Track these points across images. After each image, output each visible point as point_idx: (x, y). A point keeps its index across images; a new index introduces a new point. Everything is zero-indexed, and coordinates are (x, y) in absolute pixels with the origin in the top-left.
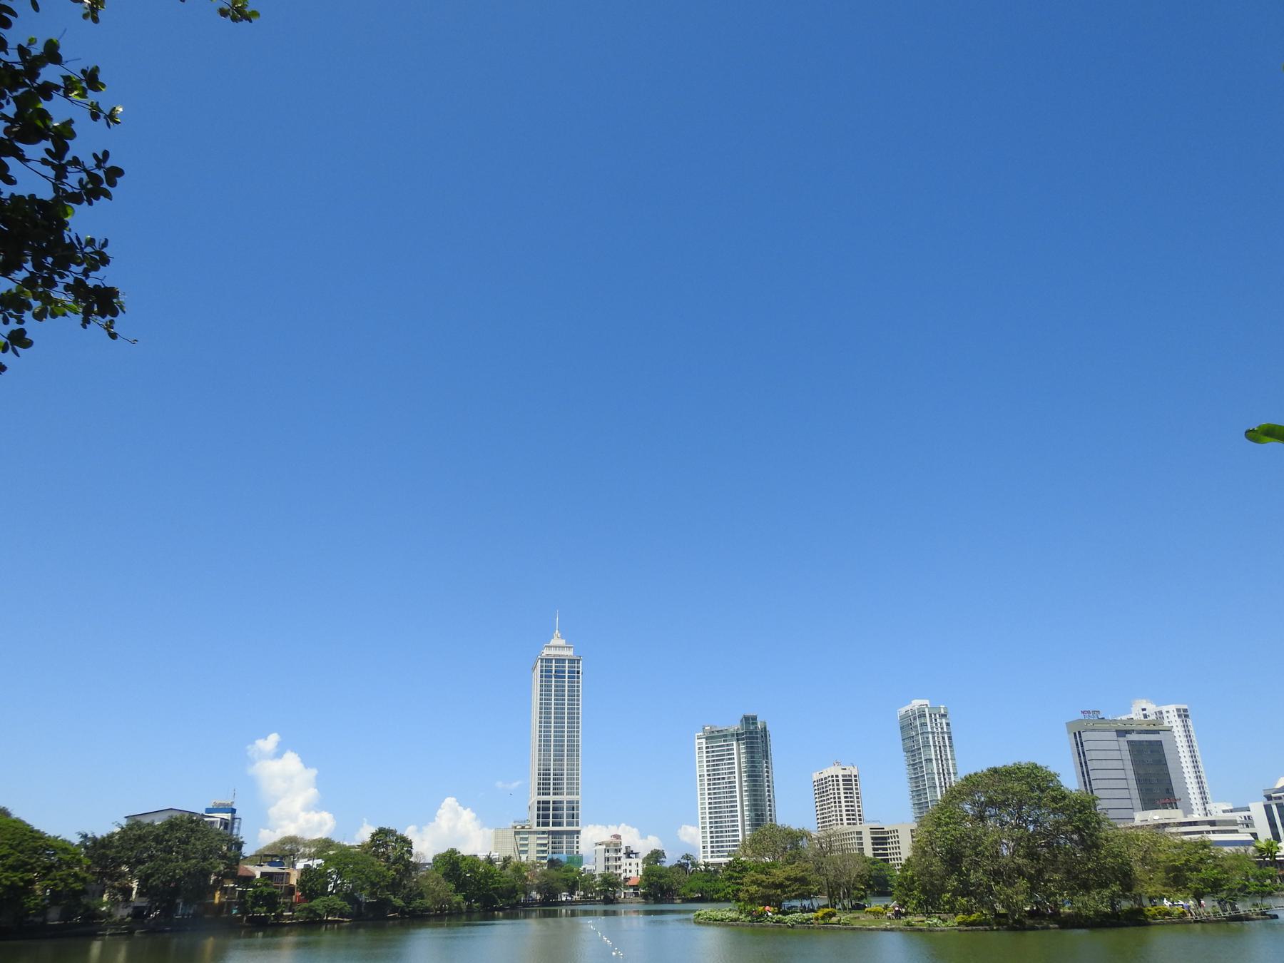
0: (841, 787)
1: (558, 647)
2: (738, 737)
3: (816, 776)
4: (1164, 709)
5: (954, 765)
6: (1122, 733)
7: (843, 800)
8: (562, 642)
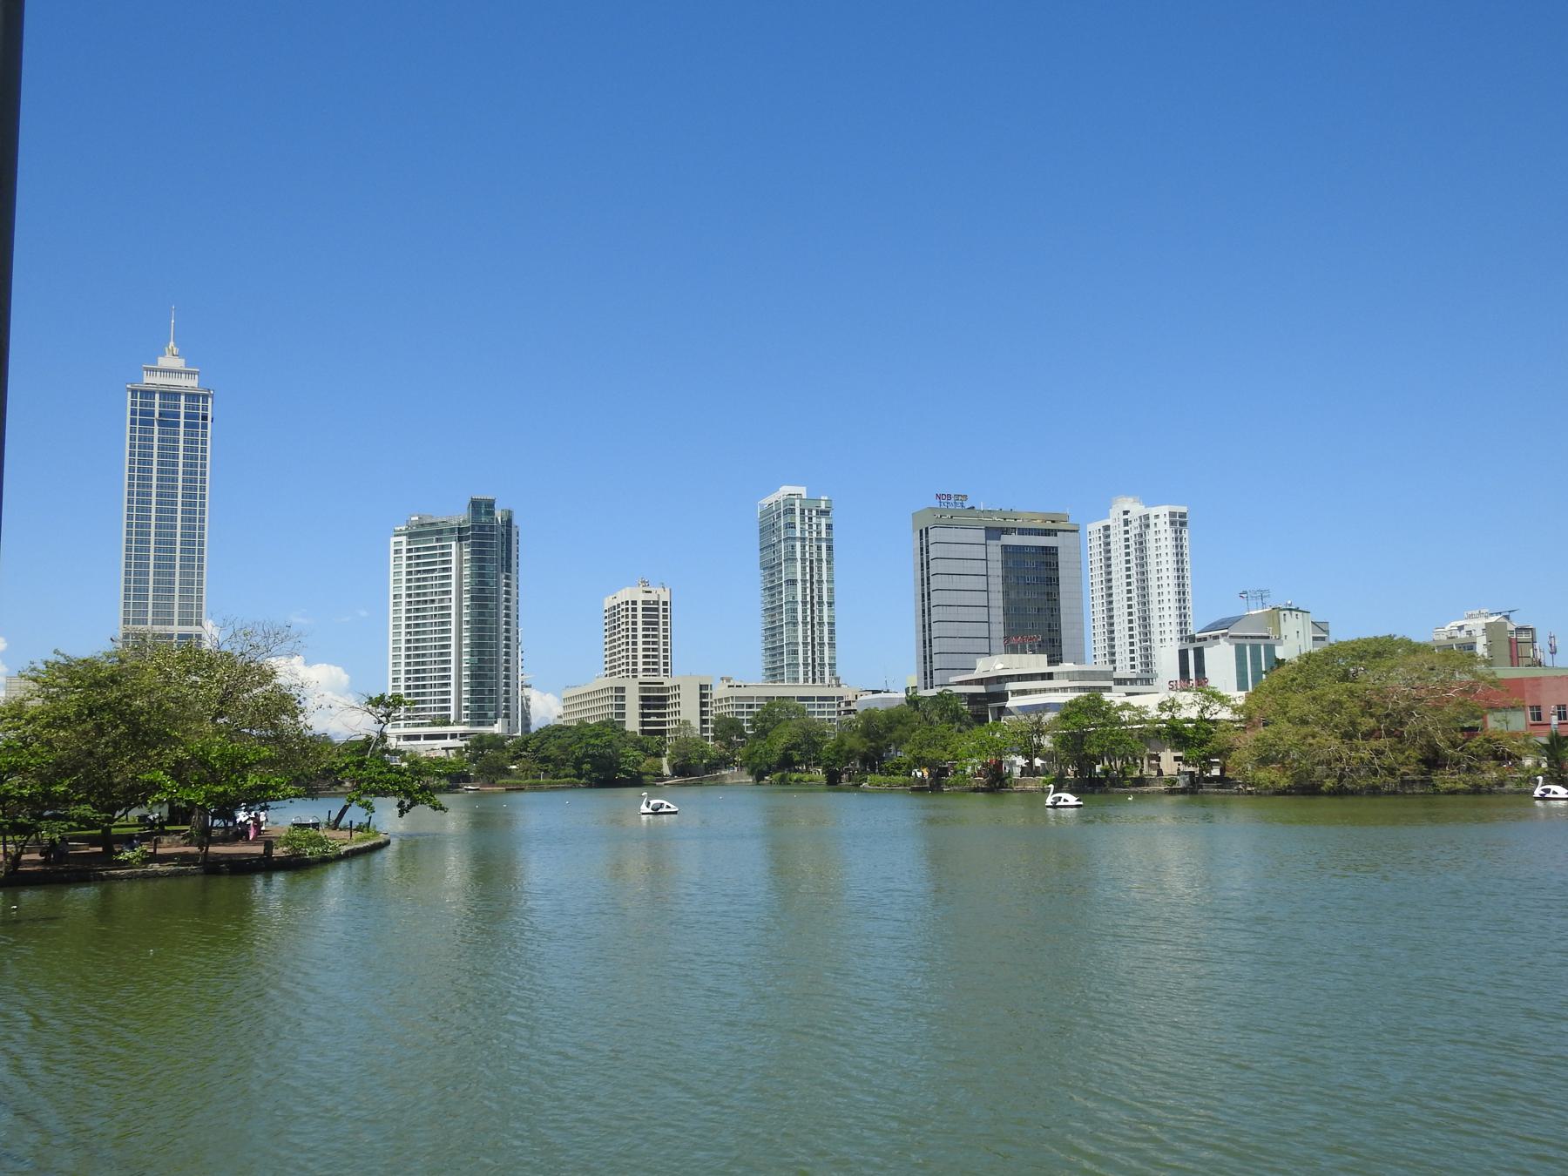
0: (640, 620)
1: (171, 369)
2: (461, 534)
3: (608, 602)
4: (1153, 511)
5: (830, 590)
6: (993, 532)
7: (640, 640)
8: (178, 363)
